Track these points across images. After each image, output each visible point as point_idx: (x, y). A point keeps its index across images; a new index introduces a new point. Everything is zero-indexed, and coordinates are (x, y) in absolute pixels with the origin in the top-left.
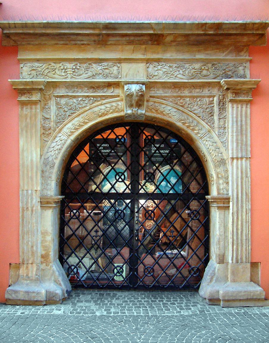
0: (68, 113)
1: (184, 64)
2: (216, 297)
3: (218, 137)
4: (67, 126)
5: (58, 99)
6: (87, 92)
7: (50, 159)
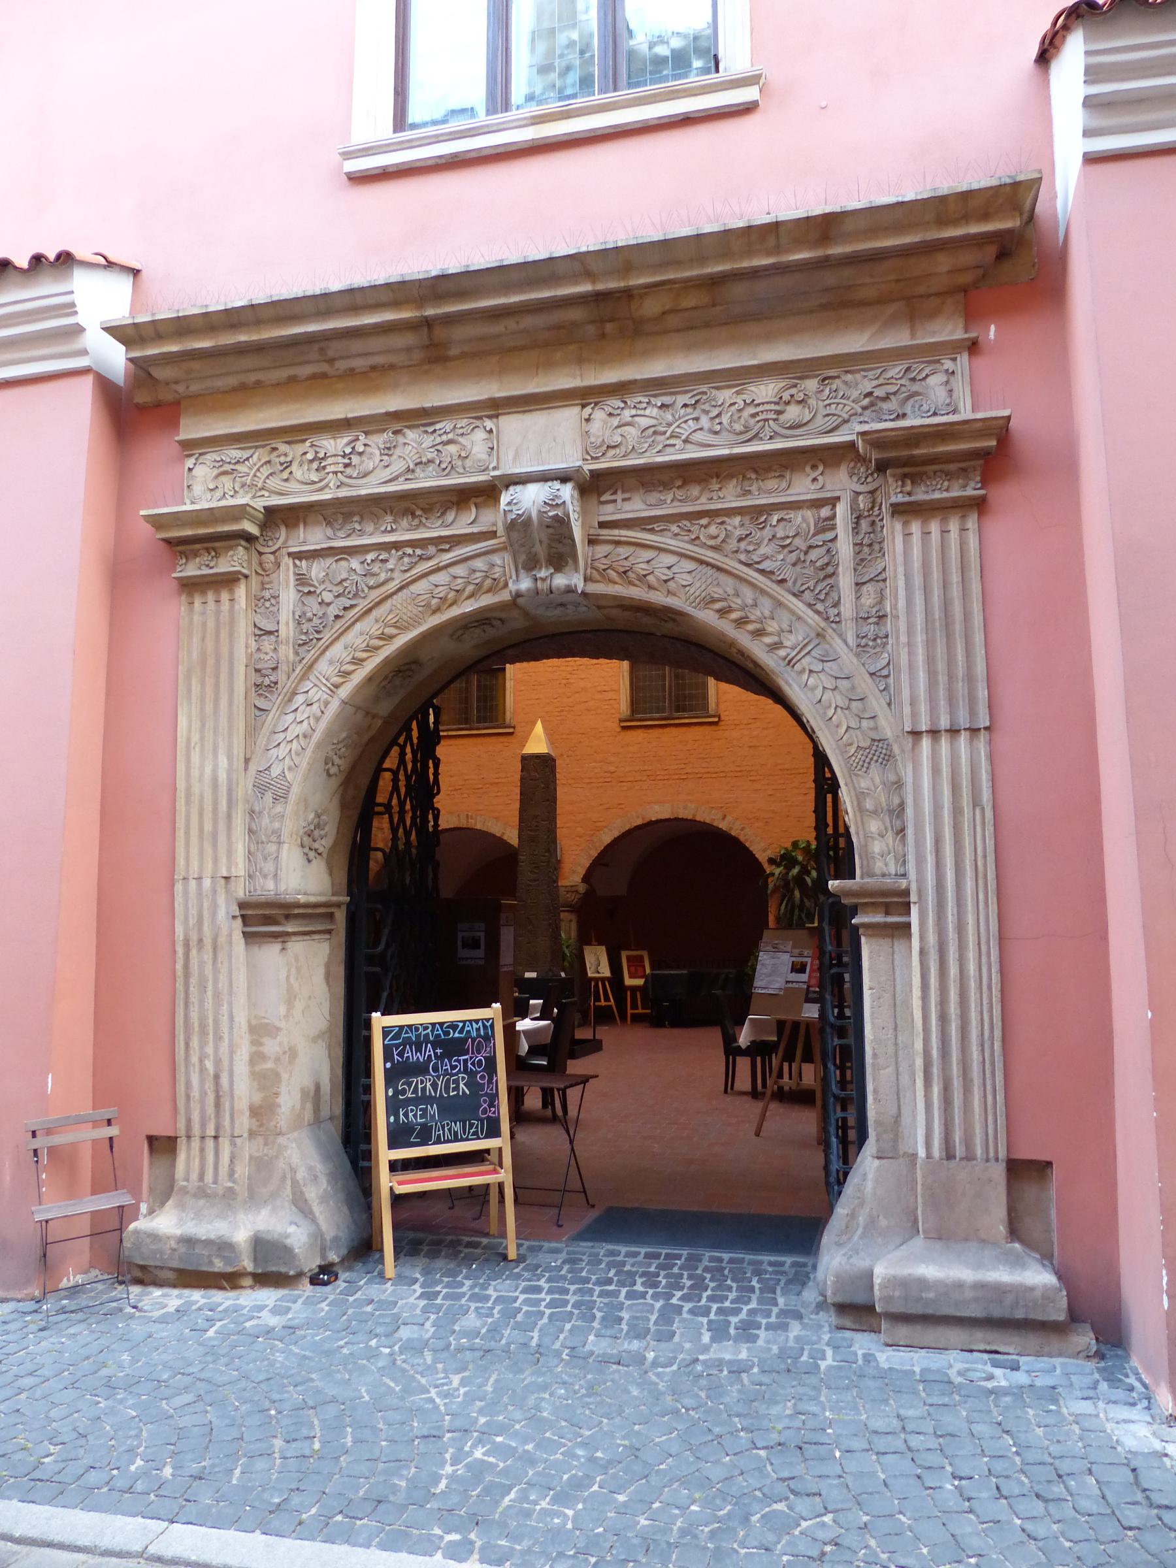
0: (333, 611)
2: (860, 1299)
3: (857, 655)
5: (304, 562)
6: (392, 530)
7: (275, 771)
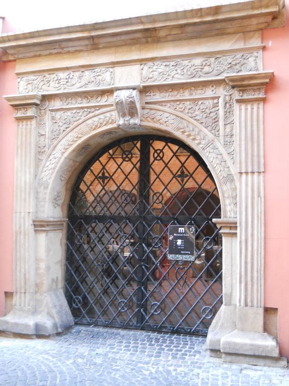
0: (62, 129)
1: (182, 61)
4: (61, 143)
